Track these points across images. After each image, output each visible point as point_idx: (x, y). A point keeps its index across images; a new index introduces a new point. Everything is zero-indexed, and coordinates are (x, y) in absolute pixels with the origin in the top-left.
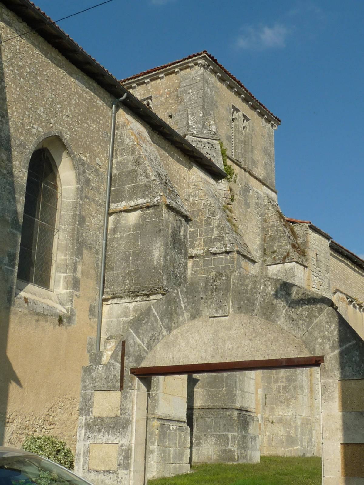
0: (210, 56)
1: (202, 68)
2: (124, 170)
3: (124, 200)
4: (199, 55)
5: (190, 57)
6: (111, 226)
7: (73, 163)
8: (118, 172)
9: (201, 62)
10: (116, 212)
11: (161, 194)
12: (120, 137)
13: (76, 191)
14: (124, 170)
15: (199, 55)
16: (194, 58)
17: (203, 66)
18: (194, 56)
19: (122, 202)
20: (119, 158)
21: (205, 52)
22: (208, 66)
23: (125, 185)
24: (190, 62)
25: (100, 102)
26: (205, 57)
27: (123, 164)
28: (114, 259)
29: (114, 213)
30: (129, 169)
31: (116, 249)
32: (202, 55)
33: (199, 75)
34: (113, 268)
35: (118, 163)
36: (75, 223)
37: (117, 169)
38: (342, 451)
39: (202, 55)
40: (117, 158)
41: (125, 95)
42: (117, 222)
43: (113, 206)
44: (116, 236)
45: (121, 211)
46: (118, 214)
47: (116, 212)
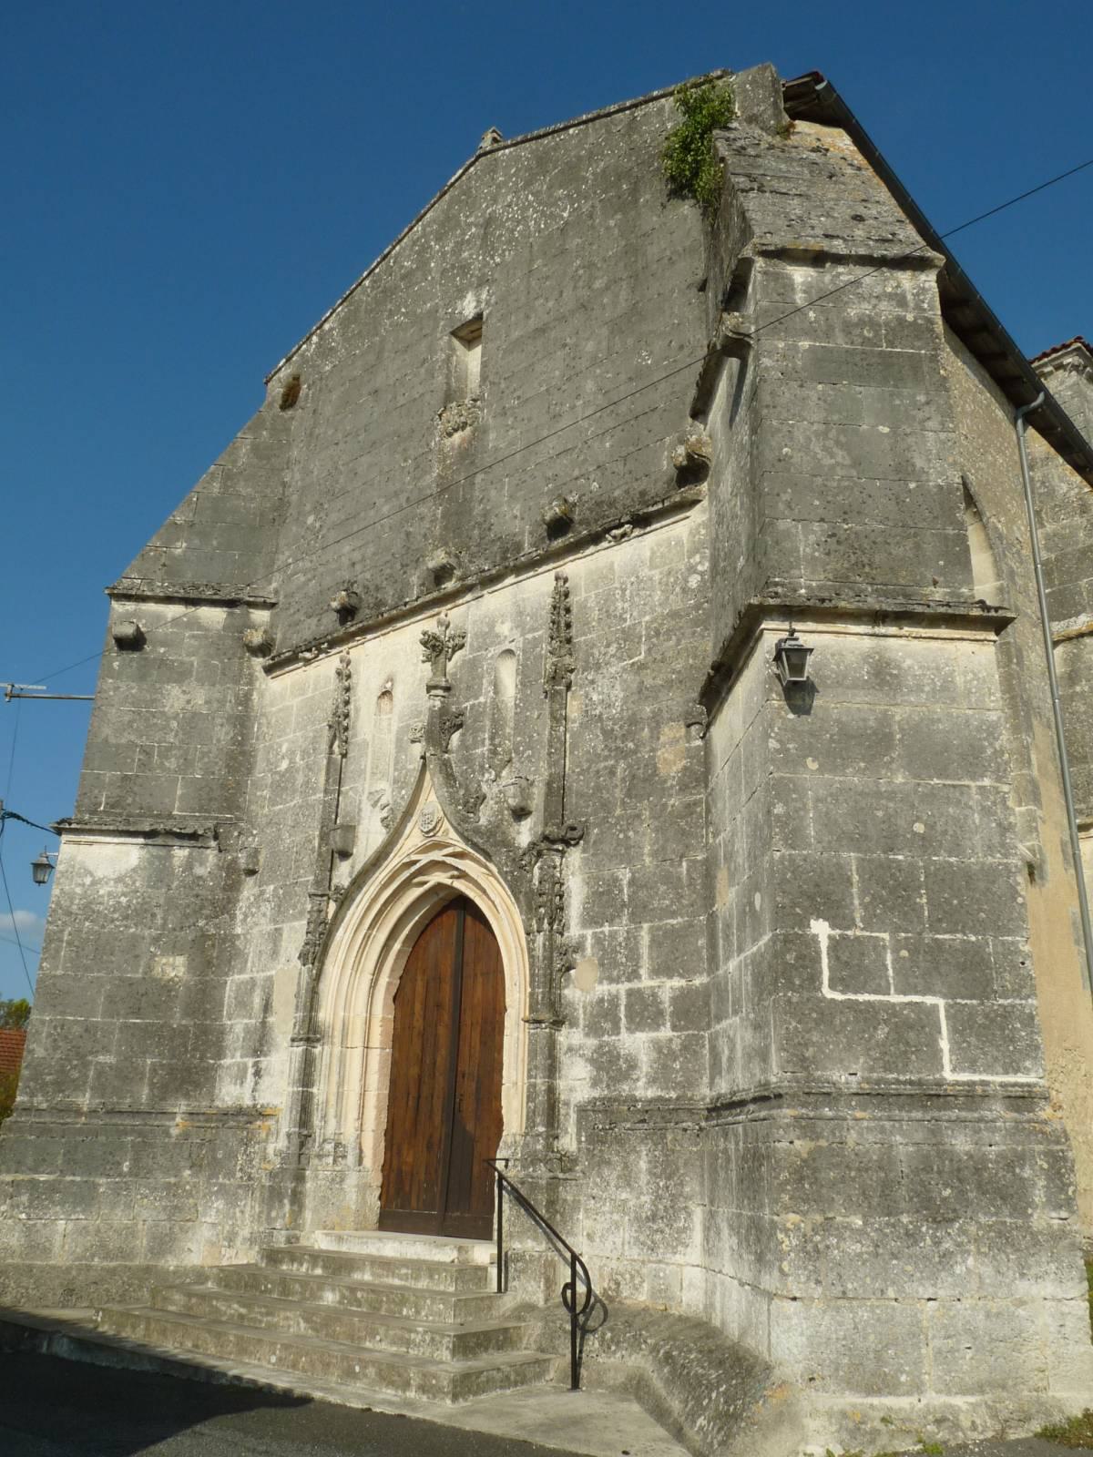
0: (1087, 347)
1: (1074, 373)
2: (1070, 549)
3: (1084, 610)
4: (1065, 346)
5: (1045, 355)
6: (1059, 669)
7: (987, 535)
8: (1053, 556)
9: (1070, 360)
10: (1069, 639)
11: (562, 729)
12: (1043, 483)
13: (997, 595)
14: (1070, 549)
15: (1065, 346)
16: (1054, 356)
17: (1075, 367)
18: (1055, 350)
19: (1077, 614)
20: (1050, 528)
21: (1078, 339)
22: (1085, 367)
23: (1078, 579)
24: (1045, 365)
25: (1000, 414)
26: (1079, 349)
27: (1063, 537)
28: (1083, 737)
29: (1063, 641)
30: (1080, 546)
31: (1084, 717)
32: (1073, 347)
33: (1070, 387)
34: (1086, 757)
35: (1048, 537)
36: (1011, 661)
37: (1049, 550)
38: (391, 1017)
39: (1073, 347)
40: (1043, 526)
41: (1041, 396)
42: (1073, 660)
43: (1058, 628)
44: (1078, 689)
45: (1082, 635)
46: (1075, 641)
47: (1069, 639)
